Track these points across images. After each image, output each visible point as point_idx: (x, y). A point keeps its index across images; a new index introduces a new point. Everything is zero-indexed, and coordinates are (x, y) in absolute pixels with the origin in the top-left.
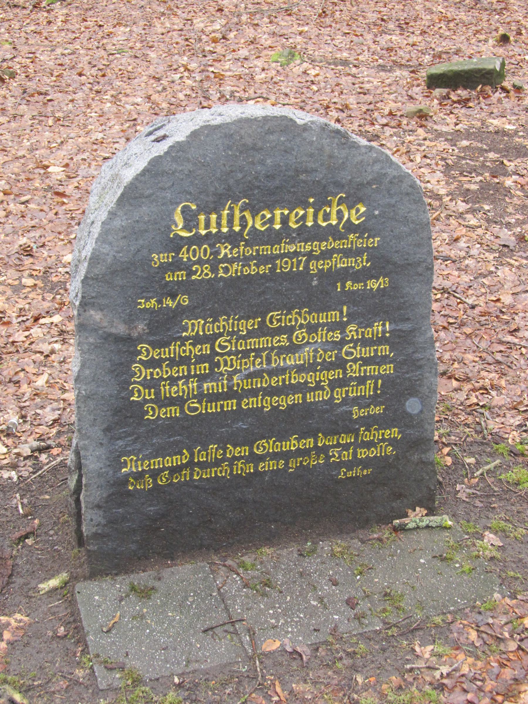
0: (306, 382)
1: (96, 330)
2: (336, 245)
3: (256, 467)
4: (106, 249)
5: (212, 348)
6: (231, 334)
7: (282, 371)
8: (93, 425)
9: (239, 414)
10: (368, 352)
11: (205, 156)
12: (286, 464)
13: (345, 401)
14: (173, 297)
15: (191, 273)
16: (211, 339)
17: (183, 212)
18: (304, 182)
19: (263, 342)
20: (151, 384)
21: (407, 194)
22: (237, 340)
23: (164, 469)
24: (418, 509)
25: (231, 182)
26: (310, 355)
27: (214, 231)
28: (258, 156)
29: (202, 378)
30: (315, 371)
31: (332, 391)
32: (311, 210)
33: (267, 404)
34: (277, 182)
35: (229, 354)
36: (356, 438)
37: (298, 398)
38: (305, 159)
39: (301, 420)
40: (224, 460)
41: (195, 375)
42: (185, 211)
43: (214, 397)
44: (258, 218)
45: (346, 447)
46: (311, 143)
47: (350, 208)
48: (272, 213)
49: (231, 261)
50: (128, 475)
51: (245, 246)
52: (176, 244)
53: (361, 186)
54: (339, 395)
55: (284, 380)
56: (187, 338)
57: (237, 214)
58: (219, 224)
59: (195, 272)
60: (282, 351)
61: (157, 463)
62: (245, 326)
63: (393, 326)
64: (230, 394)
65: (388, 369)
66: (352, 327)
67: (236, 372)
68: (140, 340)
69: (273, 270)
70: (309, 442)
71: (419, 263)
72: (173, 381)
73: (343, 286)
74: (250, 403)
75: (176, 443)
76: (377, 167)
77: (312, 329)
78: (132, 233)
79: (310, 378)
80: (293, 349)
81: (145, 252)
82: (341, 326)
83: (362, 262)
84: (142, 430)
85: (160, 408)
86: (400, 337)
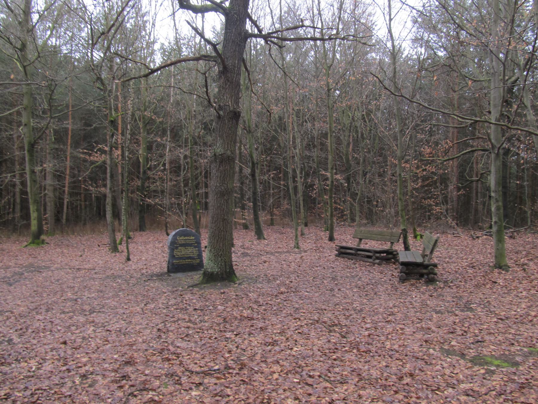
26: (190, 251)
39: (190, 258)
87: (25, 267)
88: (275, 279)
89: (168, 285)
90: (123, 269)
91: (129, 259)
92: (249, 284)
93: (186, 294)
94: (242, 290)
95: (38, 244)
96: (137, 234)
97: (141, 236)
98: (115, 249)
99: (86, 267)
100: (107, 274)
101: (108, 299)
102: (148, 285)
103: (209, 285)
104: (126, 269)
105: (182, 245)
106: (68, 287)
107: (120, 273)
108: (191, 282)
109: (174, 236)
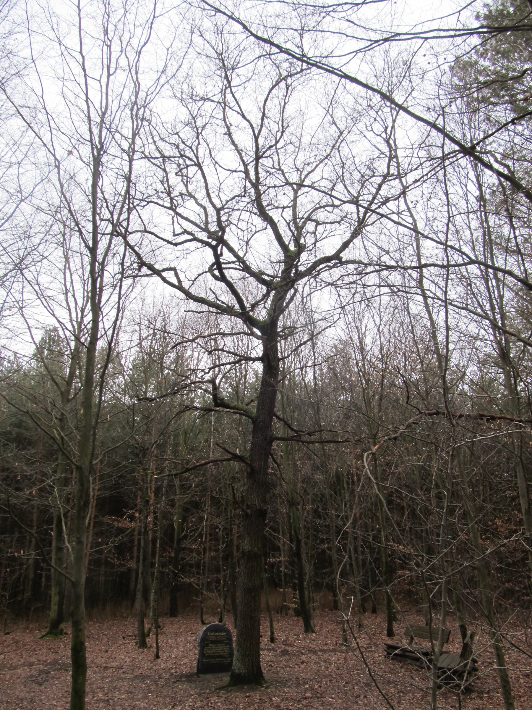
26: (221, 649)
39: (220, 657)
87: (50, 664)
88: (305, 683)
89: (196, 688)
90: (152, 667)
91: (157, 656)
92: (276, 688)
93: (213, 697)
94: (268, 694)
95: (56, 635)
96: (168, 620)
97: (172, 623)
98: (143, 644)
99: (113, 664)
100: (136, 674)
101: (138, 700)
102: (177, 687)
103: (235, 688)
104: (155, 668)
105: (213, 642)
106: (98, 688)
107: (148, 673)
108: (219, 683)
109: (205, 631)
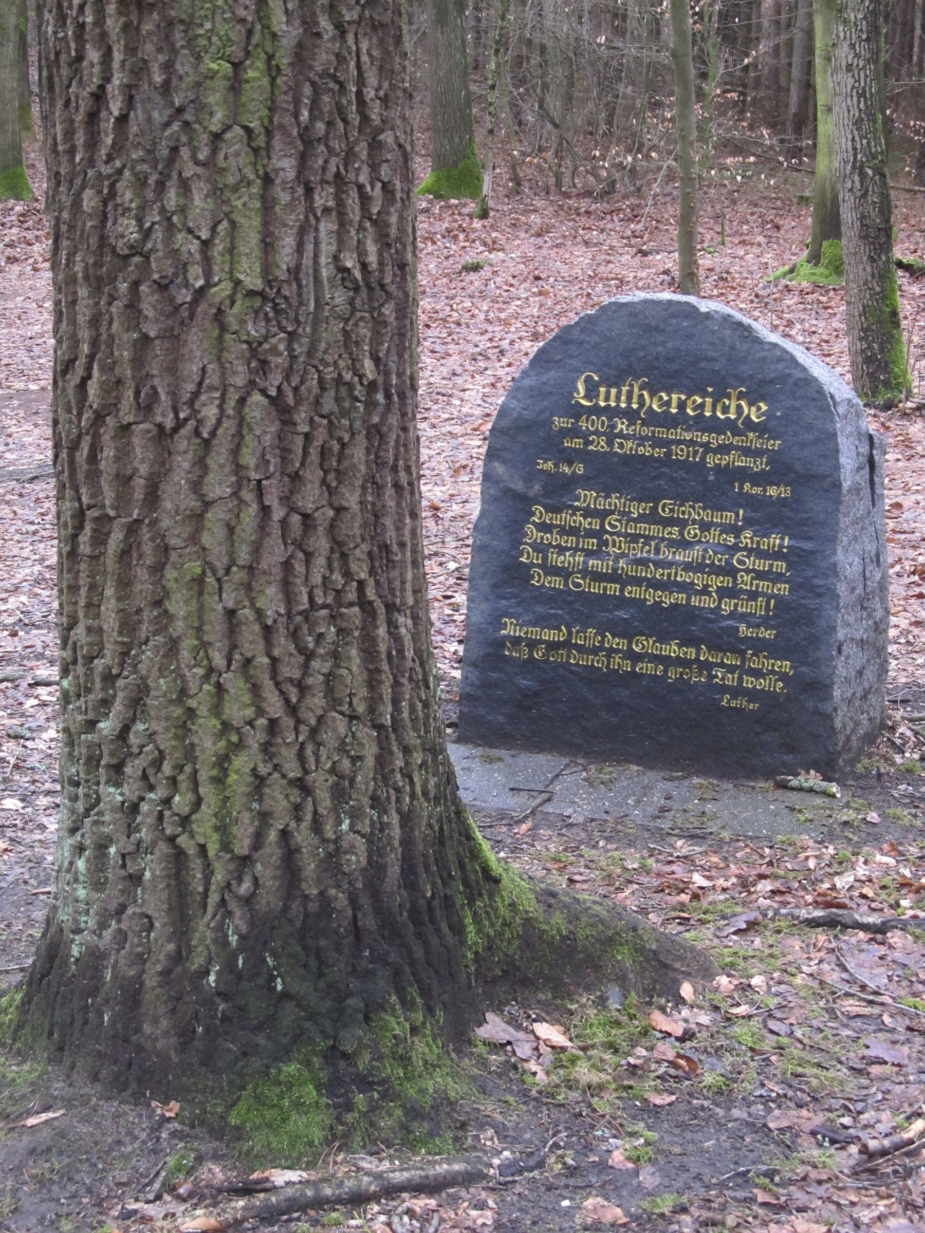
0: (692, 583)
1: (497, 482)
2: (735, 441)
3: (633, 666)
4: (514, 404)
5: (602, 525)
6: (623, 514)
7: (670, 564)
8: (482, 578)
9: (621, 602)
10: (761, 565)
11: (610, 330)
12: (665, 671)
13: (733, 615)
14: (570, 464)
15: (587, 443)
16: (603, 515)
17: (585, 381)
18: (704, 369)
19: (654, 530)
20: (540, 548)
21: (814, 400)
22: (628, 521)
23: (541, 641)
24: (812, 772)
25: (633, 359)
26: (702, 556)
27: (613, 404)
28: (660, 338)
29: (589, 554)
30: (703, 573)
31: (720, 600)
32: (709, 400)
33: (651, 597)
34: (676, 366)
35: (618, 534)
36: (743, 663)
37: (682, 598)
38: (705, 346)
40: (601, 648)
41: (583, 550)
42: (588, 380)
43: (598, 577)
44: (655, 400)
45: (731, 669)
46: (713, 332)
47: (750, 404)
48: (669, 395)
49: (627, 437)
50: (507, 637)
51: (642, 425)
52: (577, 412)
53: (763, 383)
54: (727, 607)
55: (669, 575)
56: (578, 509)
57: (636, 390)
58: (618, 399)
59: (592, 443)
60: (672, 543)
61: (535, 632)
62: (636, 510)
63: (793, 543)
64: (614, 577)
65: (783, 589)
66: (748, 533)
67: (623, 555)
68: (534, 501)
69: (668, 454)
70: (691, 653)
71: (824, 477)
72: (561, 550)
73: (741, 488)
74: (633, 592)
75: (556, 616)
76: (780, 366)
77: (705, 527)
78: (537, 393)
79: (699, 580)
80: (684, 544)
81: (547, 414)
82: (736, 531)
83: (759, 465)
84: (526, 594)
85: (546, 574)
86: (799, 556)
